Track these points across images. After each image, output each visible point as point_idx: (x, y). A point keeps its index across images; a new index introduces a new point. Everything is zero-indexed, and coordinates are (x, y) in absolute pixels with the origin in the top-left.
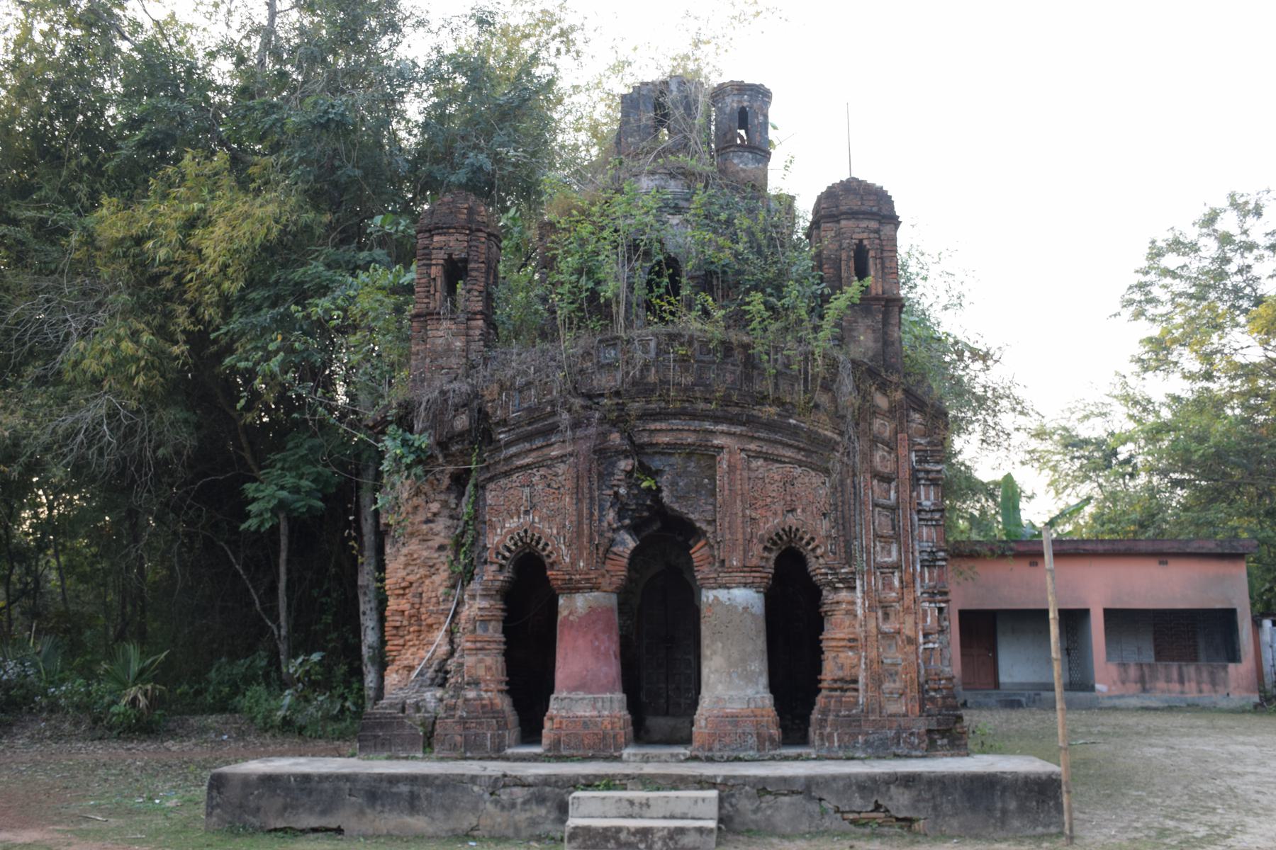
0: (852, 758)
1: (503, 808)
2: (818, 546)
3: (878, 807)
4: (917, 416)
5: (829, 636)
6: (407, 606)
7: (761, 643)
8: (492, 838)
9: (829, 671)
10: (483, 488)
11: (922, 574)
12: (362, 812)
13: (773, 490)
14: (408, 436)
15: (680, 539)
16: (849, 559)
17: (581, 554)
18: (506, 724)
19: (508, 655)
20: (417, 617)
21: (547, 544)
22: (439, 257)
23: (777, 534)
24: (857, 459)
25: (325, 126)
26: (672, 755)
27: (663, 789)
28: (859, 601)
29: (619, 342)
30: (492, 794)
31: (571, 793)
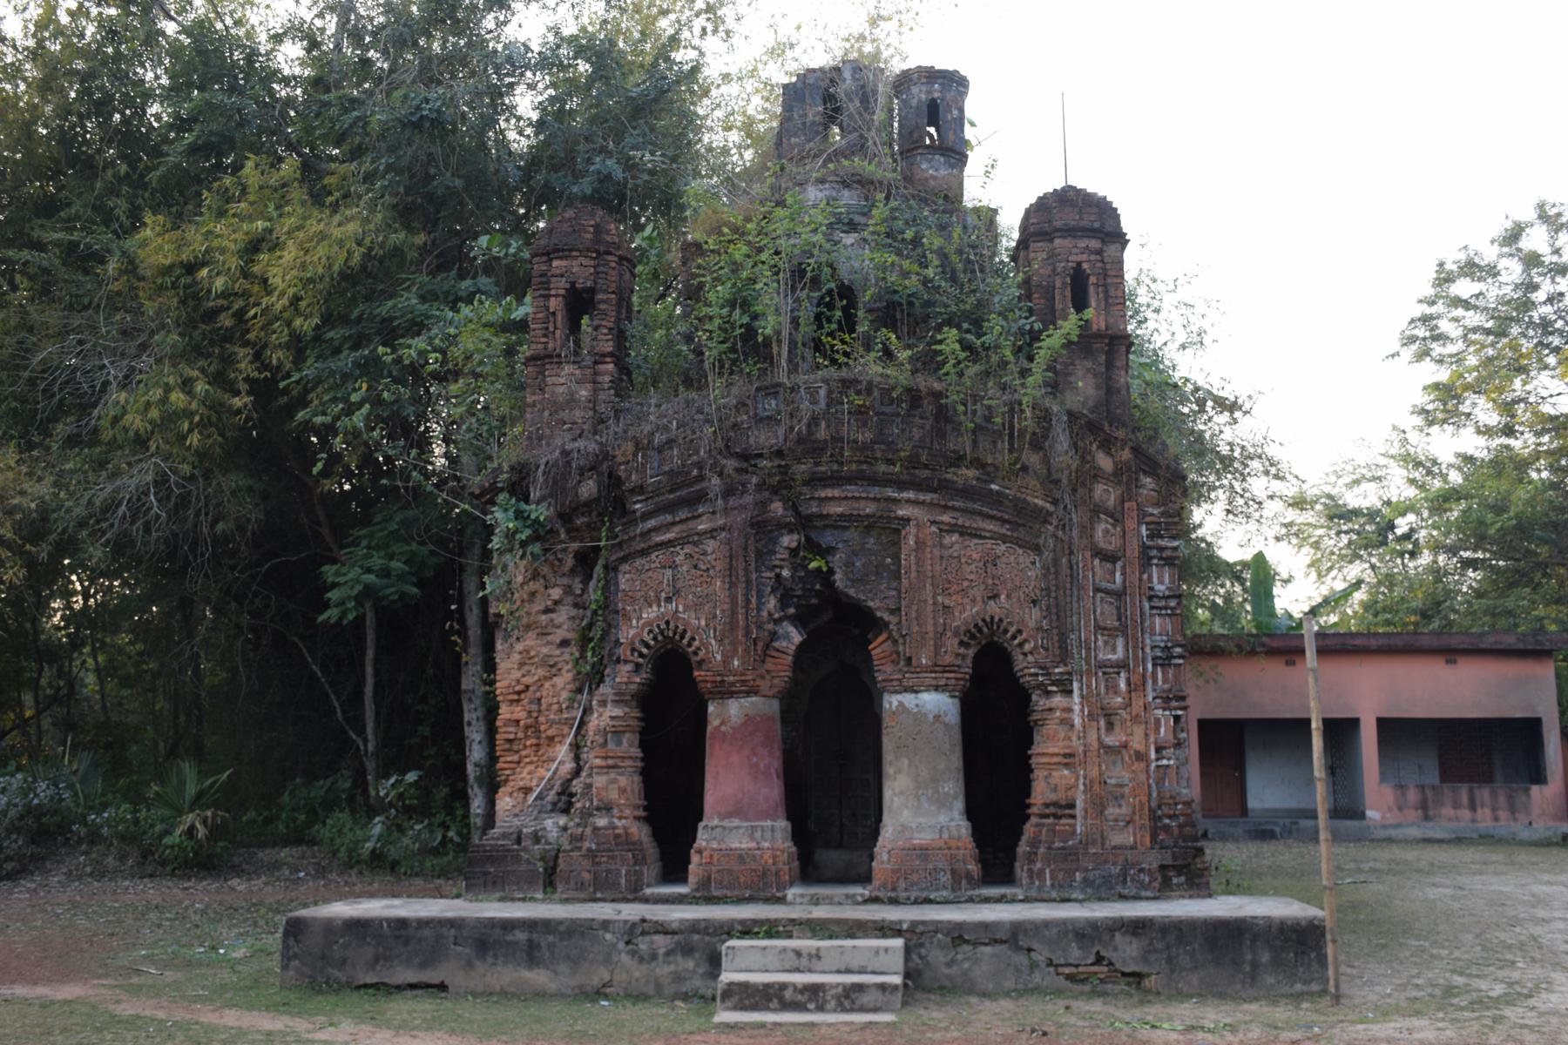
0: (1068, 900)
1: (641, 959)
2: (1025, 641)
3: (1099, 960)
4: (1147, 481)
5: (1040, 750)
6: (523, 715)
7: (956, 760)
8: (628, 996)
9: (1040, 793)
10: (616, 570)
11: (1154, 673)
12: (469, 965)
13: (971, 572)
14: (523, 506)
15: (856, 632)
16: (1064, 657)
17: (736, 650)
18: (644, 858)
19: (646, 774)
20: (534, 728)
21: (693, 639)
22: (560, 286)
23: (976, 626)
24: (1075, 533)
25: (417, 126)
26: (847, 896)
27: (837, 938)
28: (1077, 708)
29: (781, 390)
30: (627, 943)
31: (724, 942)
